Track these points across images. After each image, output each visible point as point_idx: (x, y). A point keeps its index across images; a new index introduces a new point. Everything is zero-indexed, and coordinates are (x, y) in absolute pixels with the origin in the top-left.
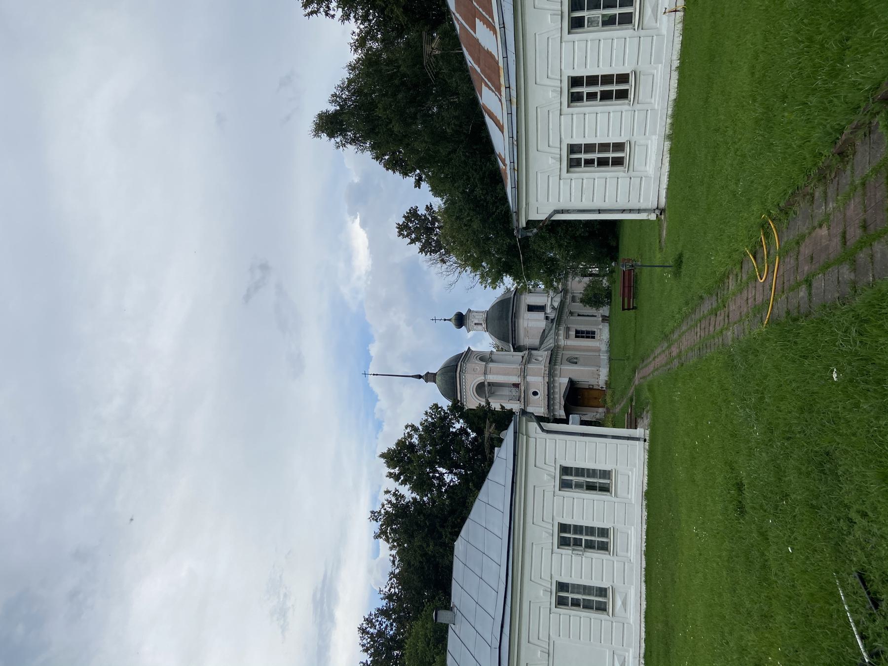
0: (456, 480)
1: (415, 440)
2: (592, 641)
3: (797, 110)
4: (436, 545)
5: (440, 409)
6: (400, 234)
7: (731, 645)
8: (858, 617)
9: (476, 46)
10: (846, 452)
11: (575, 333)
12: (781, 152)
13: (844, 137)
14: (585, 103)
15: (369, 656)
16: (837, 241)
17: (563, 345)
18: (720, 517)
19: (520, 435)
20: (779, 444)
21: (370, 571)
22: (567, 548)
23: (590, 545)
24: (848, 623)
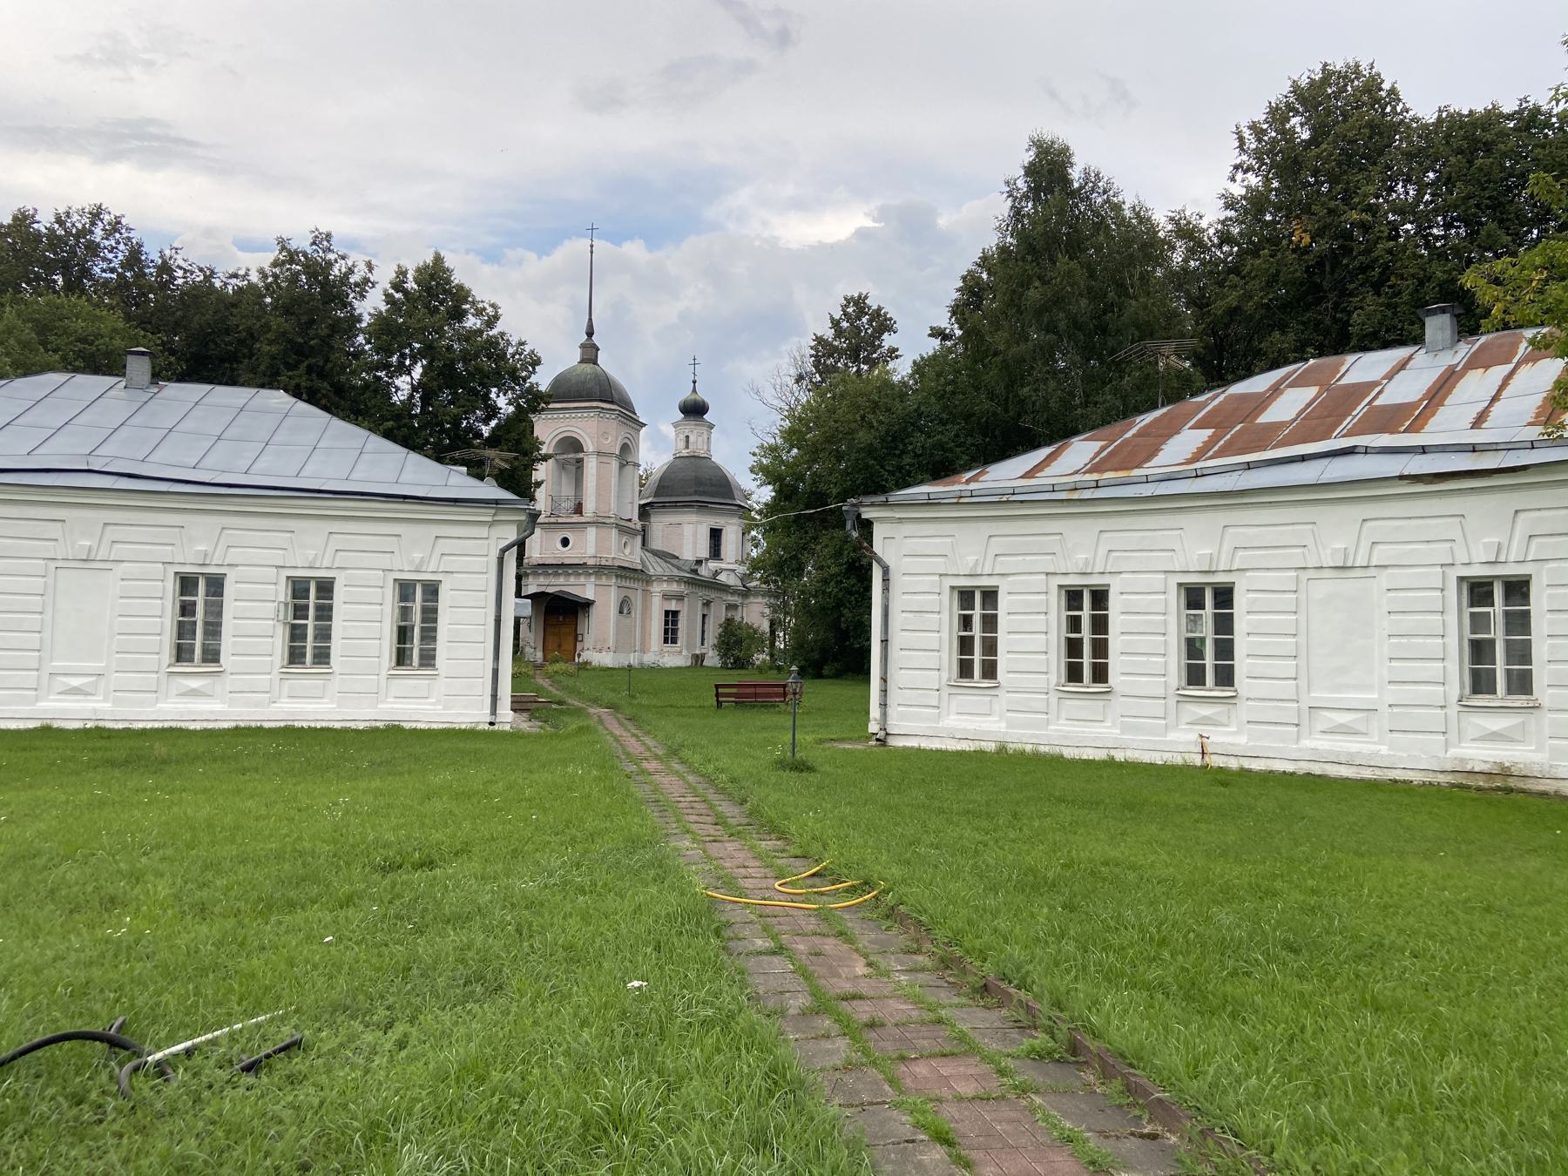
0: (399, 398)
1: (472, 322)
2: (118, 637)
3: (1053, 926)
4: (273, 358)
5: (531, 369)
6: (848, 300)
7: (144, 860)
8: (225, 1042)
9: (1169, 429)
10: (506, 1013)
11: (673, 609)
12: (985, 904)
13: (1013, 990)
14: (1065, 614)
15: (48, 225)
16: (848, 988)
17: (652, 590)
18: (371, 837)
19: (493, 511)
20: (509, 918)
21: (209, 232)
22: (290, 592)
23: (297, 634)
24: (208, 1028)
